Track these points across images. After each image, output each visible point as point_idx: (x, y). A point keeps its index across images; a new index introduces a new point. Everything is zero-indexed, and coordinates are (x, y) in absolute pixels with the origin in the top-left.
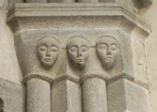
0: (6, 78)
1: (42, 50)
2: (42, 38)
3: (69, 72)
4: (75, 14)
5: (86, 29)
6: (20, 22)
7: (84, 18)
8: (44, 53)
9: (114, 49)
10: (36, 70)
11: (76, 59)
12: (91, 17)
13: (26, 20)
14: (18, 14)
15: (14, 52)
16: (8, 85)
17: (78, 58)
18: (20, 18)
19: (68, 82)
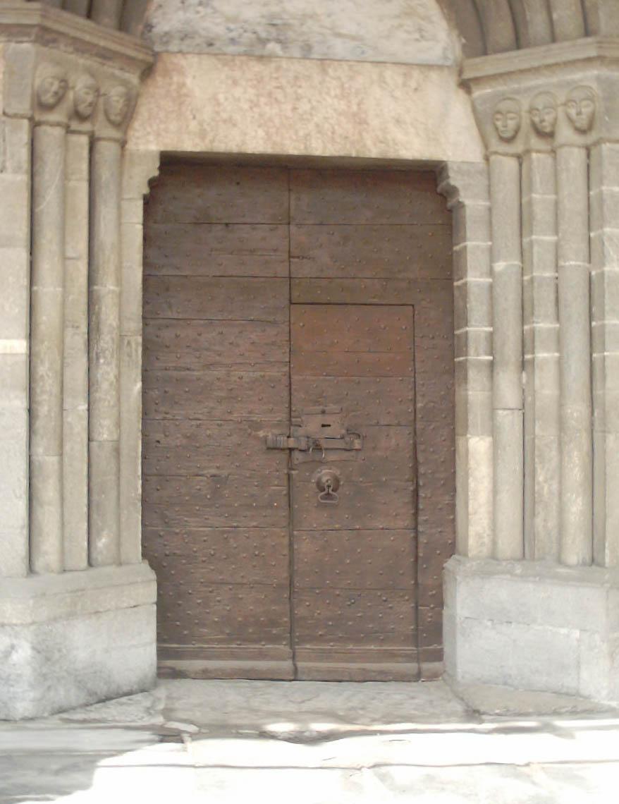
0: (460, 160)
1: (497, 120)
2: (416, 514)
3: (535, 142)
4: (536, 64)
5: (555, 80)
6: (472, 85)
7: (548, 67)
8: (499, 124)
9: (548, 113)
10: (495, 145)
11: (539, 126)
12: (557, 64)
13: (477, 80)
14: (468, 75)
15: (473, 121)
16: (465, 167)
17: (207, 141)
18: (469, 80)
19: (534, 155)
